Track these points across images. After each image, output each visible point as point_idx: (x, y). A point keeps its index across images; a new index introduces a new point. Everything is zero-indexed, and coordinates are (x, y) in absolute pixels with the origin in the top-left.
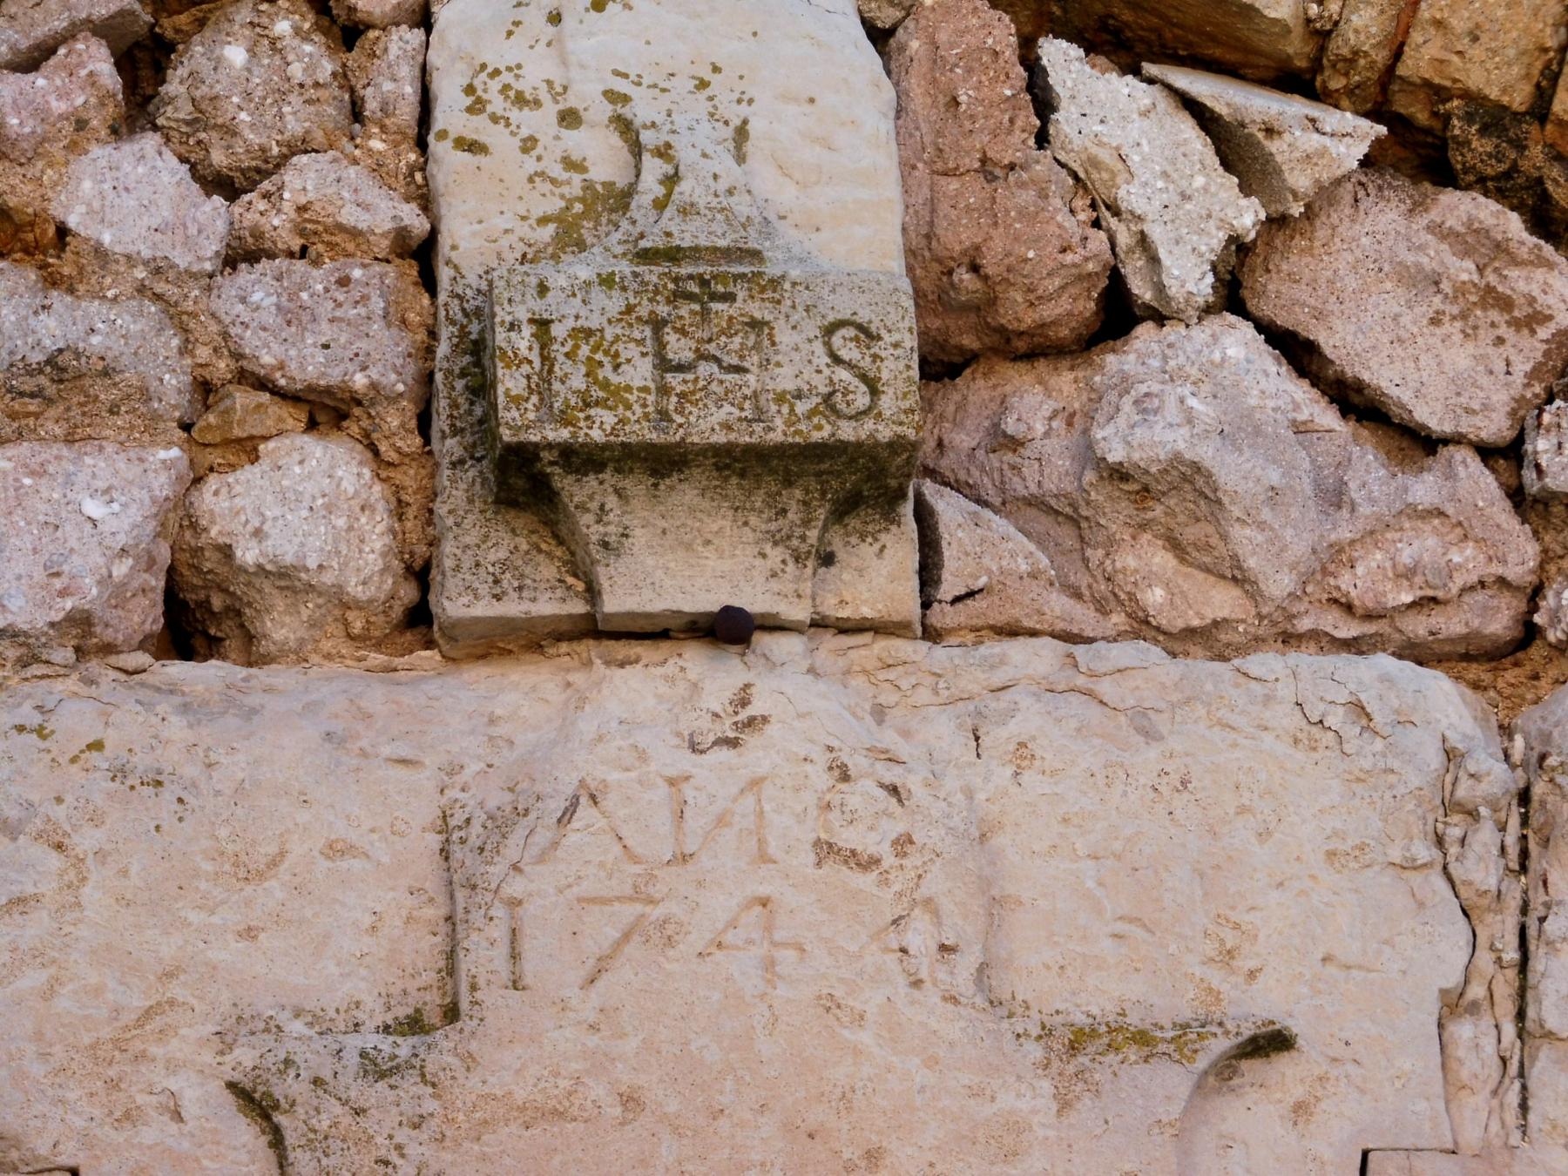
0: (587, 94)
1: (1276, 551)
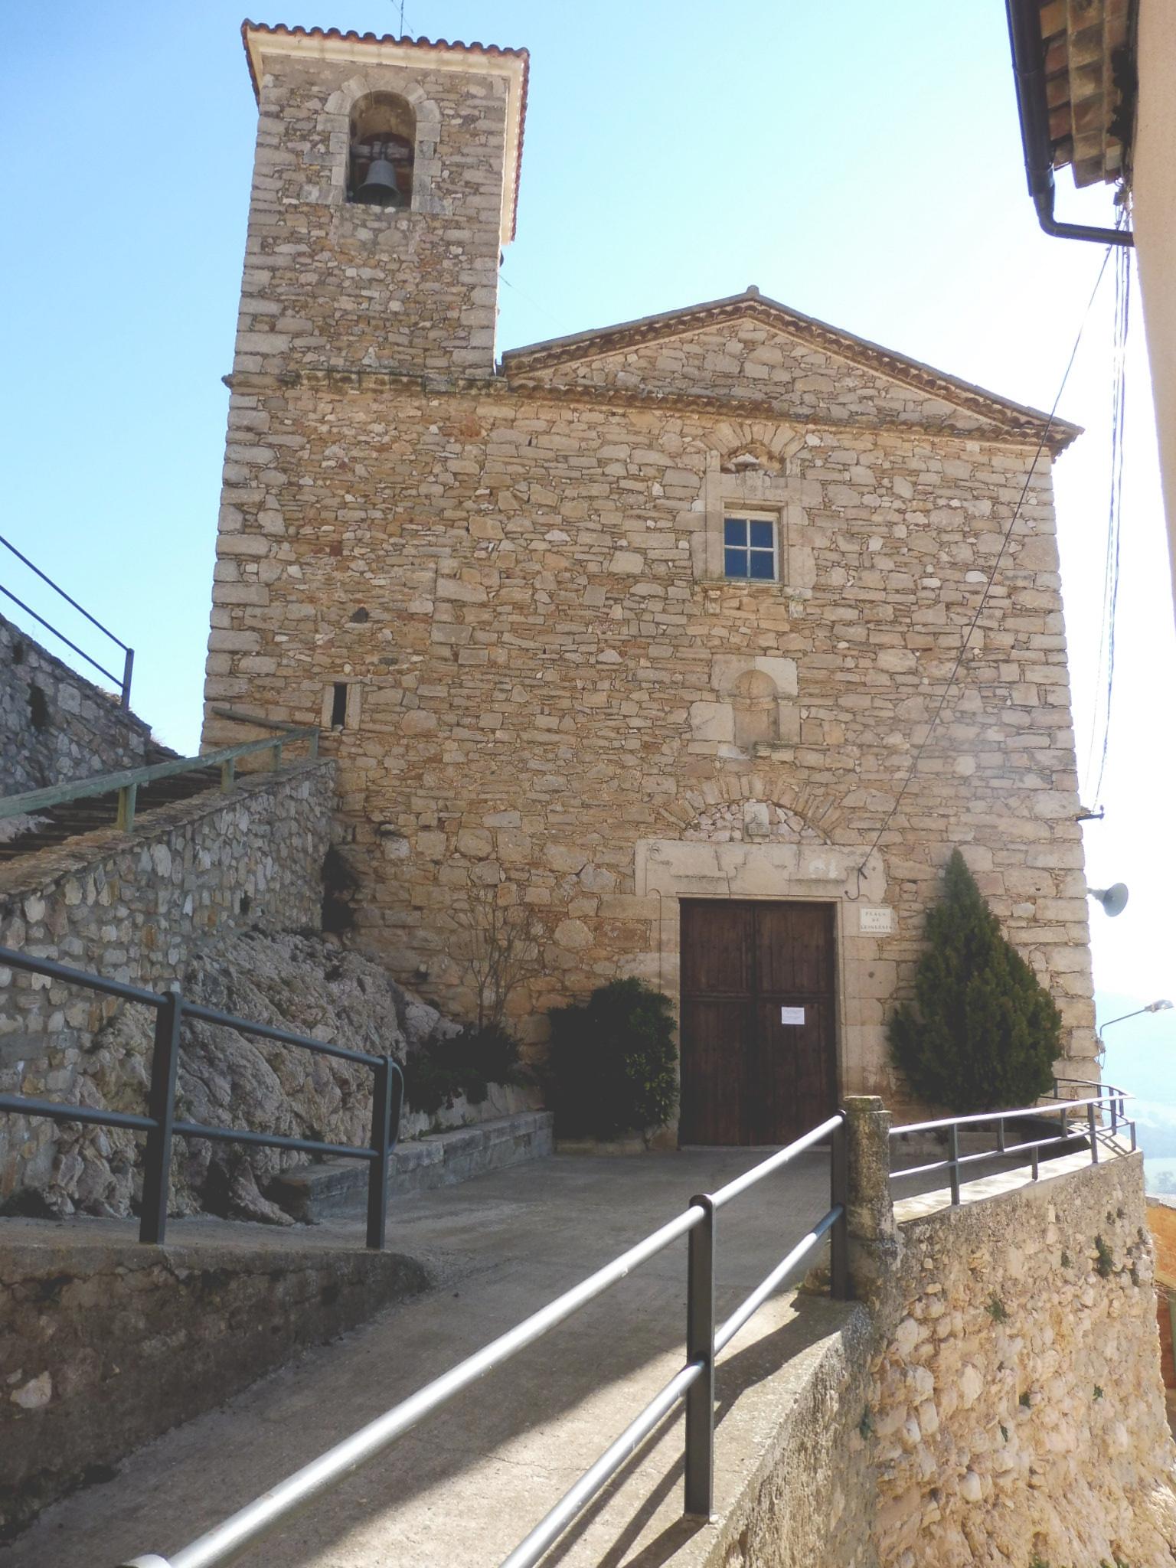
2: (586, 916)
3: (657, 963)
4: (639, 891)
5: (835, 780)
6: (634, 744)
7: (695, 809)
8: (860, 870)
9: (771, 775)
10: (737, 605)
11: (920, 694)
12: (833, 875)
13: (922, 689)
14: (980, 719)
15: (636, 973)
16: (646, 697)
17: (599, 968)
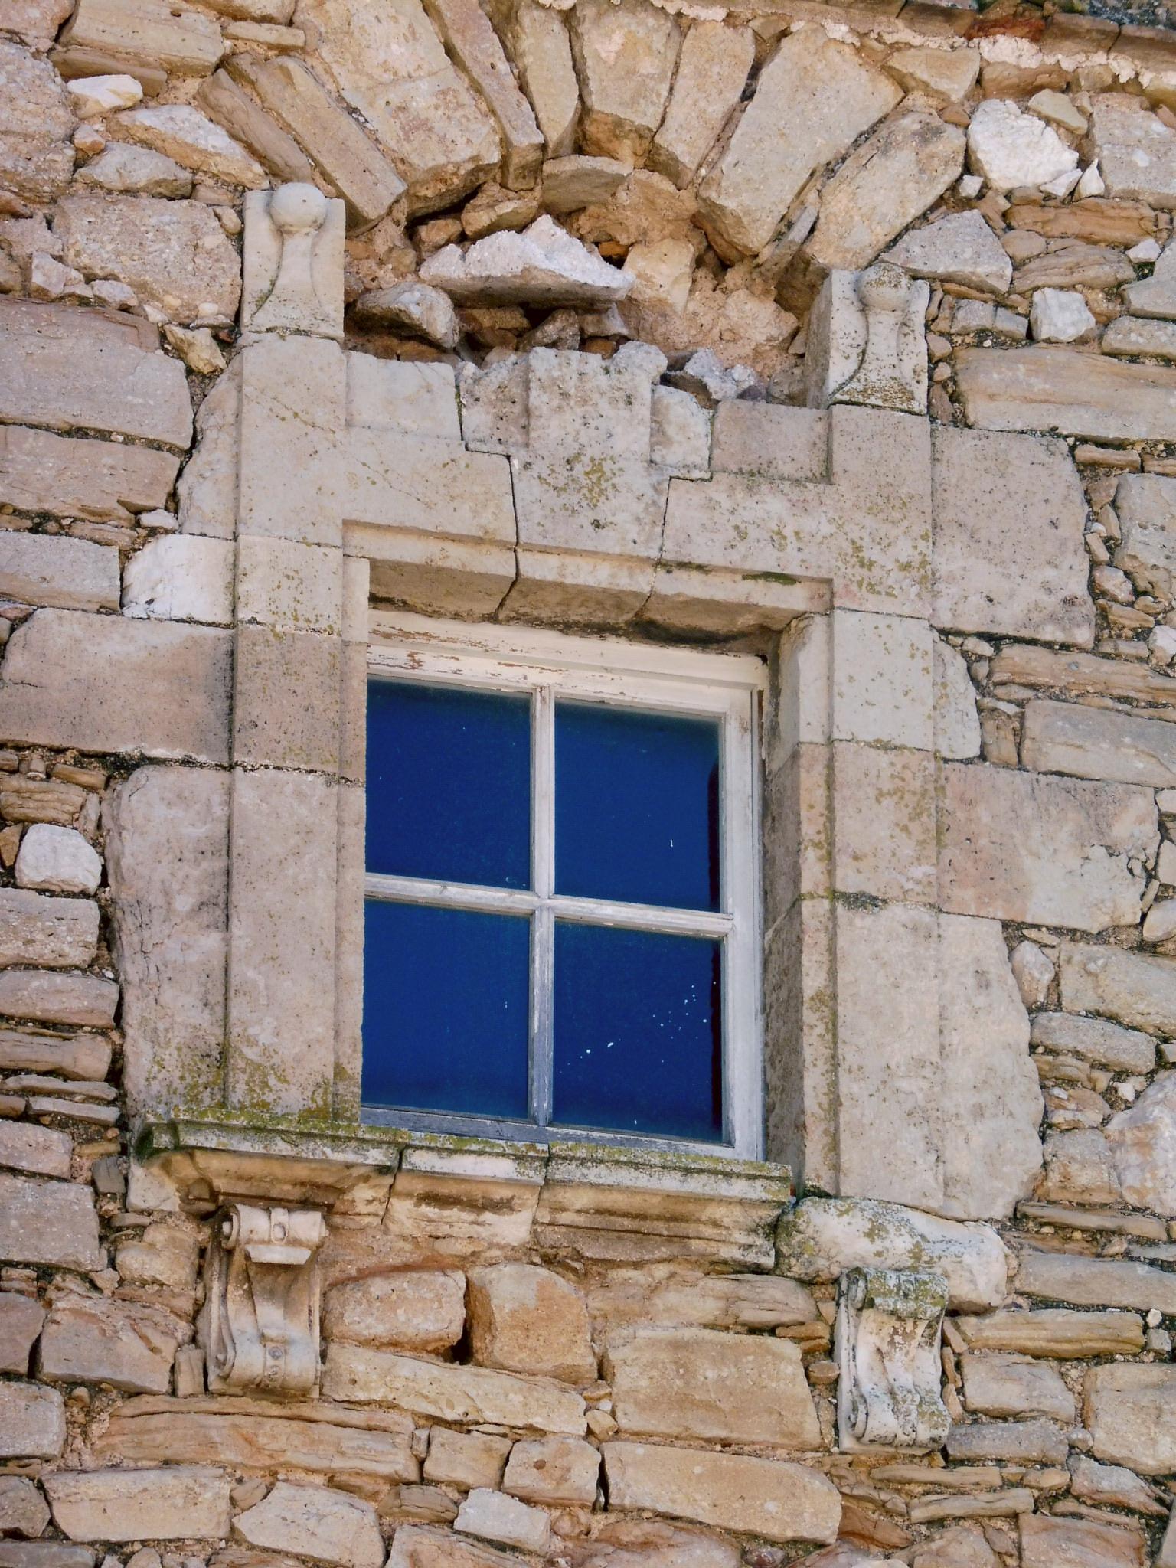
10: (448, 1322)
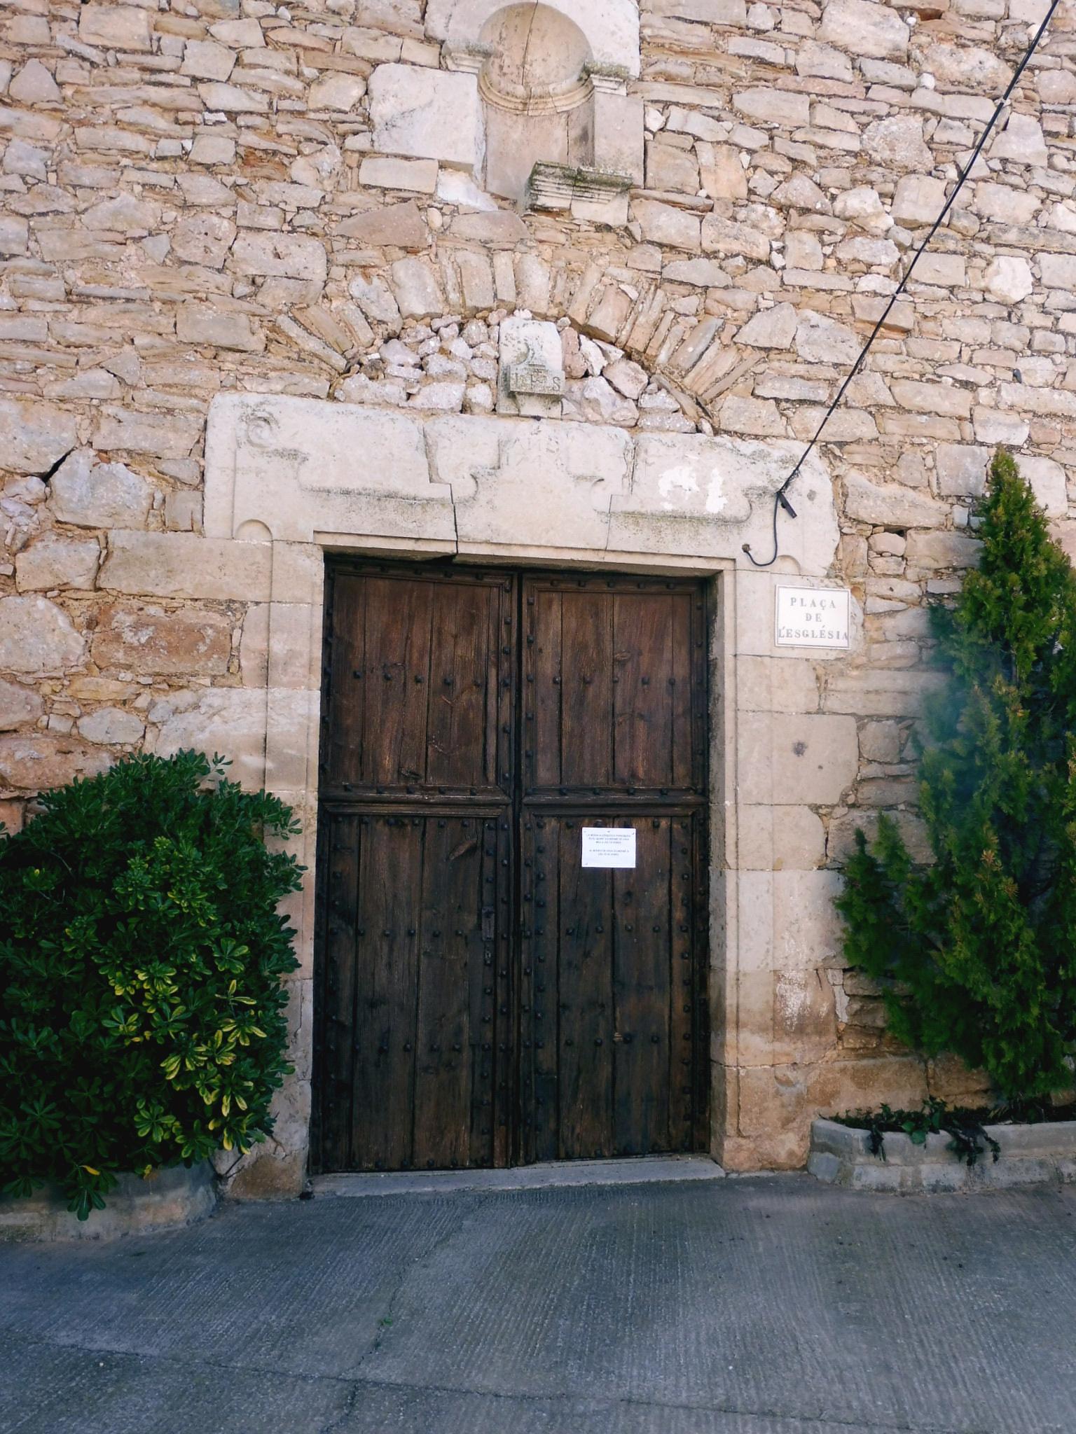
0: (521, 339)
1: (606, 411)
2: (63, 588)
3: (258, 716)
4: (215, 524)
5: (723, 279)
6: (216, 147)
7: (373, 323)
8: (779, 495)
9: (572, 254)
11: (916, 110)
12: (714, 505)
13: (919, 99)
14: (1039, 178)
15: (201, 742)
16: (256, 37)
17: (92, 728)
